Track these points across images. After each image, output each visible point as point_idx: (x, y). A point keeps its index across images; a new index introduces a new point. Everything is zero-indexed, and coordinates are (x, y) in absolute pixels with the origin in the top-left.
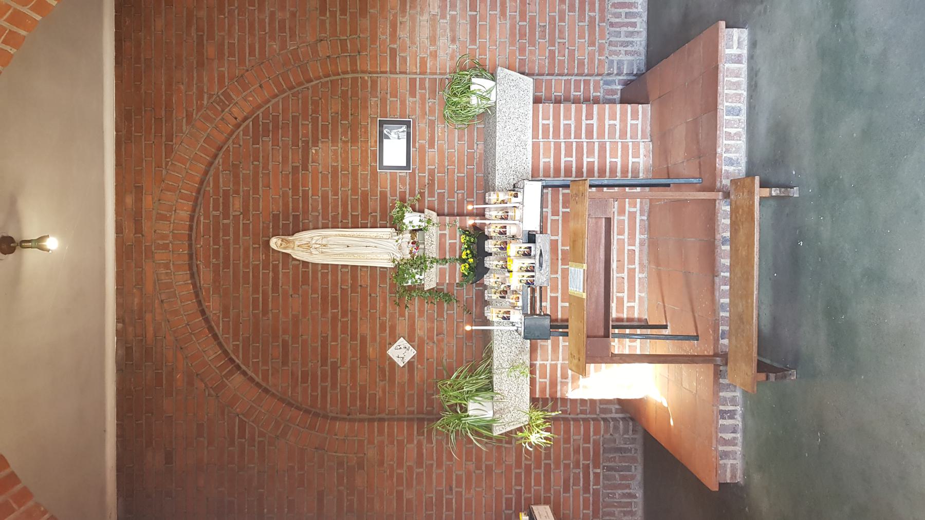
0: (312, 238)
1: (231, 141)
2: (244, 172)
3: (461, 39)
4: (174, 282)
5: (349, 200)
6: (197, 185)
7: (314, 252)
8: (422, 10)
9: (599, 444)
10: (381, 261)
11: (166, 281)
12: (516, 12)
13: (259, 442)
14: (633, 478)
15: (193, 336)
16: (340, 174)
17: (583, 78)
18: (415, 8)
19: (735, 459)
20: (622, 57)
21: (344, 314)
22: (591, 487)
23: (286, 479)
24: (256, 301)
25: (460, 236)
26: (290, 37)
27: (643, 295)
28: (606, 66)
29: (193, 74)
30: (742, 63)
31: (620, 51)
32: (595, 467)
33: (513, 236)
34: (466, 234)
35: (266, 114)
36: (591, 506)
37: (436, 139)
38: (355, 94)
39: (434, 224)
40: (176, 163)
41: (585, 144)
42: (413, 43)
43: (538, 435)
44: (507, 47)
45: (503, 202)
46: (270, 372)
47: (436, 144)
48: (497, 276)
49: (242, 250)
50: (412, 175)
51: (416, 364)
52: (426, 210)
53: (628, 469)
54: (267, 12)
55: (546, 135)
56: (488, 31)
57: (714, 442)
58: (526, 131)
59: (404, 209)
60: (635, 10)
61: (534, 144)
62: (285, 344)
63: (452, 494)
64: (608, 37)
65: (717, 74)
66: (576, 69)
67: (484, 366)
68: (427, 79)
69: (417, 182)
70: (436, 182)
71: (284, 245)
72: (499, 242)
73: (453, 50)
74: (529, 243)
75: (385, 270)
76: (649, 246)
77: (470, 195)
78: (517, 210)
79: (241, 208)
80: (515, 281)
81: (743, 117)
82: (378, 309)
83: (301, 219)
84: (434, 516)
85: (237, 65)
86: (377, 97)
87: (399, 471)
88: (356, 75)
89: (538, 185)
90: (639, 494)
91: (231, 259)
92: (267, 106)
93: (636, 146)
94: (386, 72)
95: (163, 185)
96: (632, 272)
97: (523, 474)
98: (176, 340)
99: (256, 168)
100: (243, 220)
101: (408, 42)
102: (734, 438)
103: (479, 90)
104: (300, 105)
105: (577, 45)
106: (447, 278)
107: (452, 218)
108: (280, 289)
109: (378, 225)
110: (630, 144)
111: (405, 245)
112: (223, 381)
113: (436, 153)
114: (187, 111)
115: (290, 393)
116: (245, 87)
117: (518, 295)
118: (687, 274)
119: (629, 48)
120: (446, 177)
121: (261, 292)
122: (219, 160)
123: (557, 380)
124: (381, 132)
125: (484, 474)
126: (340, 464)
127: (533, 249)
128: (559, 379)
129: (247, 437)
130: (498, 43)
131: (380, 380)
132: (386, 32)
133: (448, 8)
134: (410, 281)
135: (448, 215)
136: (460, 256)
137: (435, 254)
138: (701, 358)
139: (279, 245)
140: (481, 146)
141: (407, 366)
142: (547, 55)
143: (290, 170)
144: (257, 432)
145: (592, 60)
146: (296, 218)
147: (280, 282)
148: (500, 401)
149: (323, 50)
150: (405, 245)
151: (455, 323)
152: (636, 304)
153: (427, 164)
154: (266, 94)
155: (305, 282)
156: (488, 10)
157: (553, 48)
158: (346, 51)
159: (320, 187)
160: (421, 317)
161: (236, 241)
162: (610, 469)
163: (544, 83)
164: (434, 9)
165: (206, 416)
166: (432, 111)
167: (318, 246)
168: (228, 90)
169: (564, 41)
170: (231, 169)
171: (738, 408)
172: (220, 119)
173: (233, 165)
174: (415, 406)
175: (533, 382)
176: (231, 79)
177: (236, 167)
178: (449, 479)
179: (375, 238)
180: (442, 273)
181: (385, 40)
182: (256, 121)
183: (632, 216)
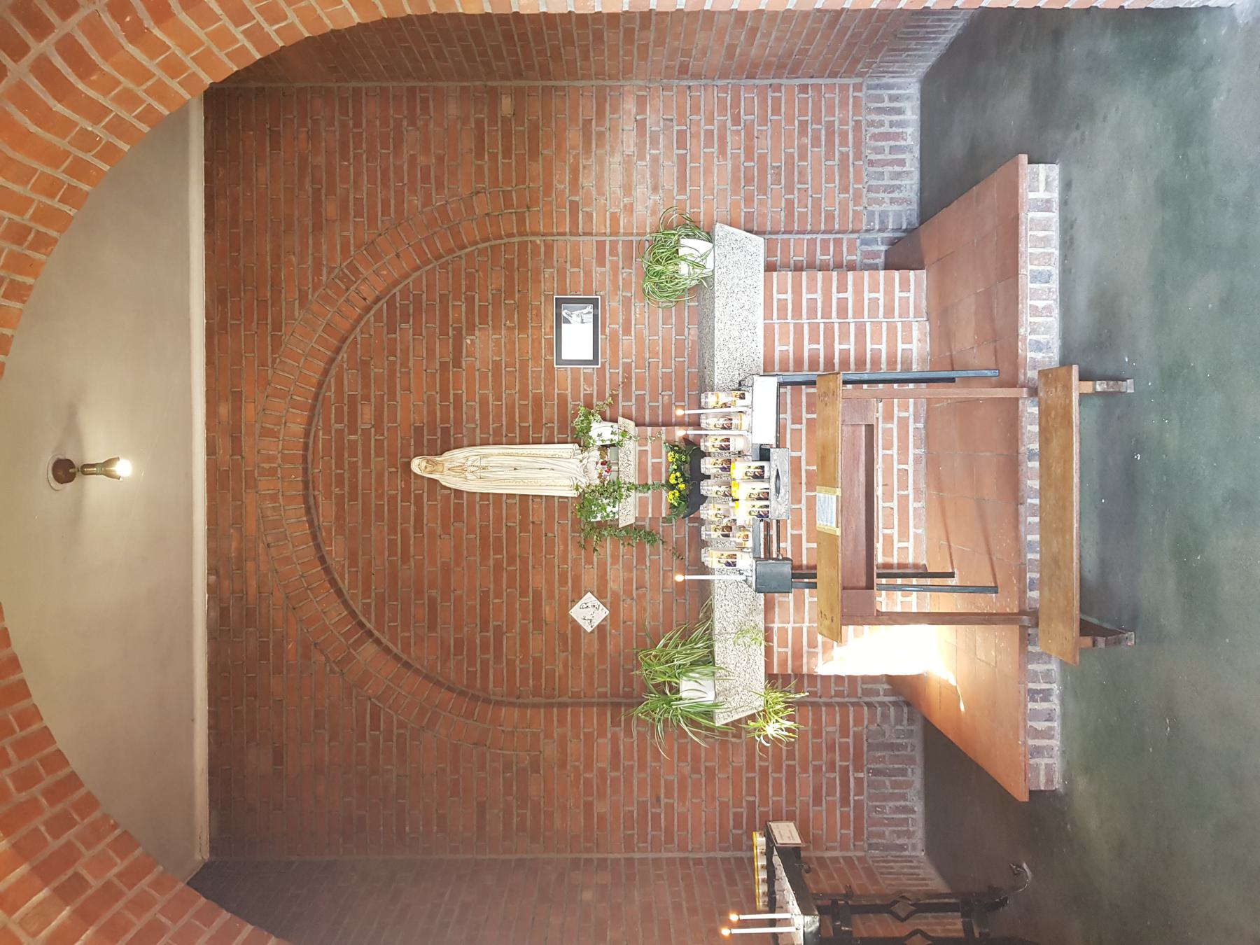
1: (358, 329)
2: (376, 370)
5: (517, 406)
7: (470, 477)
12: (740, 149)
14: (909, 785)
16: (503, 371)
18: (603, 146)
20: (886, 207)
21: (511, 561)
22: (851, 798)
24: (392, 543)
25: (667, 453)
26: (437, 189)
27: (920, 531)
28: (865, 219)
31: (883, 198)
32: (857, 770)
34: (675, 450)
35: (405, 293)
39: (631, 437)
40: (287, 360)
41: (836, 326)
42: (601, 193)
43: (777, 725)
44: (729, 197)
45: (725, 405)
47: (633, 329)
48: (718, 506)
50: (602, 372)
51: (608, 627)
52: (620, 419)
54: (406, 157)
57: (1022, 733)
59: (591, 417)
60: (903, 143)
61: (766, 326)
62: (432, 601)
63: (660, 806)
64: (866, 180)
66: (823, 225)
67: (701, 630)
68: (620, 242)
69: (608, 381)
70: (633, 381)
74: (761, 460)
76: (927, 462)
80: (743, 513)
81: (1055, 285)
82: (556, 553)
85: (366, 228)
86: (553, 267)
88: (525, 238)
89: (773, 382)
90: (919, 807)
91: (360, 488)
93: (907, 327)
95: (269, 389)
96: (903, 500)
101: (594, 193)
103: (691, 255)
105: (823, 192)
106: (650, 510)
107: (656, 429)
109: (556, 440)
110: (899, 325)
111: (592, 466)
112: (350, 653)
113: (634, 341)
114: (299, 290)
115: (439, 668)
116: (377, 257)
117: (747, 533)
118: (980, 503)
119: (896, 195)
120: (647, 374)
121: (399, 532)
122: (343, 355)
124: (559, 315)
126: (508, 766)
127: (766, 469)
128: (805, 648)
129: (382, 729)
130: (715, 191)
131: (560, 651)
133: (648, 146)
134: (599, 515)
135: (650, 425)
136: (667, 481)
137: (633, 479)
138: (1002, 617)
139: (423, 468)
140: (694, 331)
142: (783, 205)
143: (438, 367)
144: (395, 722)
145: (844, 211)
146: (446, 431)
147: (425, 518)
150: (592, 466)
152: (910, 545)
153: (621, 356)
154: (405, 266)
155: (458, 517)
157: (792, 197)
161: (366, 463)
162: (877, 772)
164: (628, 147)
166: (627, 285)
167: (475, 469)
169: (806, 186)
170: (359, 368)
171: (1055, 686)
173: (361, 360)
175: (769, 652)
176: (358, 247)
177: (365, 364)
178: (655, 787)
180: (642, 504)
182: (391, 303)
183: (903, 423)
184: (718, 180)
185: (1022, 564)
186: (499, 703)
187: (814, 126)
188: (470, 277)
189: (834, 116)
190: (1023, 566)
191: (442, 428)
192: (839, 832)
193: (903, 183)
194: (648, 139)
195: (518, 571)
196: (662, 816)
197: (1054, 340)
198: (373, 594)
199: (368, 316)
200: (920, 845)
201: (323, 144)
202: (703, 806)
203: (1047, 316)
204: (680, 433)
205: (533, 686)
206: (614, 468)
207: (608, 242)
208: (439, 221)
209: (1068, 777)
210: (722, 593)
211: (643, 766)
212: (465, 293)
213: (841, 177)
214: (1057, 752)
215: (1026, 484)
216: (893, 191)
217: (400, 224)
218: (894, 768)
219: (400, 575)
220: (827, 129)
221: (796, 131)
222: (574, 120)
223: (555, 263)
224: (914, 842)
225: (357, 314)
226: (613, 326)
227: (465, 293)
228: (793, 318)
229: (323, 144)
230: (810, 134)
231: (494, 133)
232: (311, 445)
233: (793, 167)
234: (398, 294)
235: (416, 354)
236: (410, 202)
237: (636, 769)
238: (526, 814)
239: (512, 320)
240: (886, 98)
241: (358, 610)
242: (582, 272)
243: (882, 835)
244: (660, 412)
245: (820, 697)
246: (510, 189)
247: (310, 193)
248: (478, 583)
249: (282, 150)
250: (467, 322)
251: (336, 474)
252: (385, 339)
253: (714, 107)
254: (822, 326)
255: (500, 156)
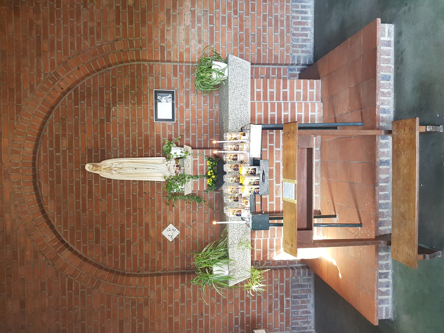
0: (112, 164)
1: (60, 103)
2: (69, 123)
3: (204, 41)
4: (23, 193)
5: (137, 140)
6: (37, 131)
7: (114, 172)
8: (180, 23)
9: (289, 283)
10: (157, 177)
11: (18, 192)
12: (237, 26)
13: (82, 292)
14: (308, 302)
15: (36, 227)
16: (130, 124)
17: (276, 67)
18: (176, 21)
19: (388, 304)
20: (300, 54)
21: (135, 211)
22: (285, 309)
23: (99, 314)
24: (78, 203)
25: (206, 161)
26: (97, 38)
27: (318, 196)
28: (291, 59)
29: (34, 61)
30: (391, 47)
31: (299, 50)
32: (287, 297)
33: (241, 161)
34: (210, 160)
35: (83, 86)
36: (285, 319)
37: (190, 103)
38: (139, 74)
39: (190, 154)
40: (24, 117)
41: (283, 104)
42: (175, 42)
43: (257, 286)
44: (232, 47)
45: (236, 139)
46: (88, 248)
47: (190, 105)
48: (232, 187)
49: (68, 172)
50: (176, 125)
51: (180, 239)
52: (185, 146)
53: (306, 297)
54: (82, 23)
55: (259, 98)
56: (220, 37)
57: (376, 293)
58: (247, 95)
59: (171, 145)
60: (307, 26)
61: (251, 103)
62: (97, 230)
63: (203, 318)
64: (291, 42)
65: (376, 53)
66: (273, 61)
67: (223, 243)
68: (184, 66)
69: (179, 129)
70: (191, 129)
71: (94, 168)
72: (233, 165)
73: (200, 48)
74: (254, 165)
75: (160, 182)
76: (321, 165)
77: (211, 136)
78: (244, 145)
79: (67, 145)
80: (246, 191)
81: (392, 82)
82: (156, 206)
83: (106, 152)
84: (192, 331)
85: (63, 55)
86: (153, 76)
87: (170, 306)
88: (140, 63)
89: (260, 128)
90: (312, 311)
91: (62, 178)
92: (83, 82)
93: (313, 105)
94: (158, 61)
95: (15, 131)
97: (245, 303)
98: (26, 230)
99: (77, 120)
100: (69, 153)
101: (172, 42)
102: (388, 291)
103: (217, 69)
104: (105, 81)
105: (273, 46)
106: (199, 187)
107: (201, 150)
108: (93, 196)
109: (155, 155)
111: (172, 168)
112: (57, 255)
113: (190, 111)
114: (30, 84)
115: (101, 260)
116: (68, 69)
117: (247, 200)
118: (351, 185)
119: (304, 49)
120: (197, 126)
121: (81, 198)
122: (53, 115)
123: (267, 249)
124: (156, 98)
125: (222, 305)
126: (133, 303)
127: (257, 170)
128: (268, 249)
129: (73, 290)
130: (227, 44)
131: (158, 250)
132: (158, 36)
133: (196, 22)
134: (175, 190)
135: (198, 149)
136: (207, 174)
137: (191, 173)
138: (371, 242)
139: (91, 168)
140: (217, 107)
141: (174, 241)
142: (256, 52)
143: (99, 122)
144: (80, 286)
145: (282, 55)
146: (103, 151)
147: (93, 191)
148: (233, 264)
149: (118, 46)
150: (172, 168)
151: (203, 214)
153: (185, 117)
154: (82, 73)
155: (109, 191)
156: (220, 24)
157: (260, 48)
158: (133, 47)
159: (118, 132)
160: (183, 211)
161: (65, 166)
162: (295, 297)
163: (254, 69)
164: (187, 22)
165: (47, 277)
166: (187, 86)
167: (116, 169)
168: (57, 71)
169: (266, 44)
170: (61, 121)
171: (390, 271)
172: (52, 89)
173: (62, 118)
174: (180, 265)
175: (252, 252)
176: (59, 64)
177: (63, 120)
178: (201, 308)
179: (153, 163)
180: (195, 185)
181: (157, 41)
182: (76, 91)
184: (228, 39)
185: (377, 214)
186: (129, 275)
187: (269, 17)
188: (114, 80)
189: (278, 13)
190: (377, 215)
191: (101, 150)
192: (279, 323)
193: (307, 44)
194: (196, 19)
195: (138, 215)
196: (204, 321)
197: (391, 108)
198: (69, 227)
199: (65, 97)
200: (313, 327)
201: (41, 15)
202: (222, 316)
203: (388, 97)
204: (215, 152)
205: (145, 266)
206: (182, 168)
207: (178, 66)
208: (98, 53)
209: (396, 312)
210: (232, 225)
211: (195, 301)
212: (111, 87)
213: (281, 40)
214: (390, 301)
215: (379, 177)
216: (303, 47)
217: (79, 54)
218: (302, 295)
219: (81, 218)
220: (275, 19)
221: (262, 19)
222: (162, 9)
223: (154, 75)
224: (310, 325)
225: (59, 96)
226: (181, 104)
227: (111, 87)
228: (263, 100)
229: (41, 15)
230: (267, 20)
231: (125, 13)
232: (37, 158)
233: (261, 35)
234: (79, 87)
235: (88, 115)
236: (84, 43)
237: (192, 301)
238: (142, 324)
239: (134, 101)
240: (300, 7)
241: (61, 234)
242: (166, 79)
243: (297, 323)
244: (203, 143)
245: (271, 266)
246: (132, 39)
247: (35, 38)
248: (119, 221)
249: (21, 16)
250: (112, 101)
251: (50, 171)
252: (73, 108)
253: (226, 6)
254: (276, 104)
255: (127, 24)
